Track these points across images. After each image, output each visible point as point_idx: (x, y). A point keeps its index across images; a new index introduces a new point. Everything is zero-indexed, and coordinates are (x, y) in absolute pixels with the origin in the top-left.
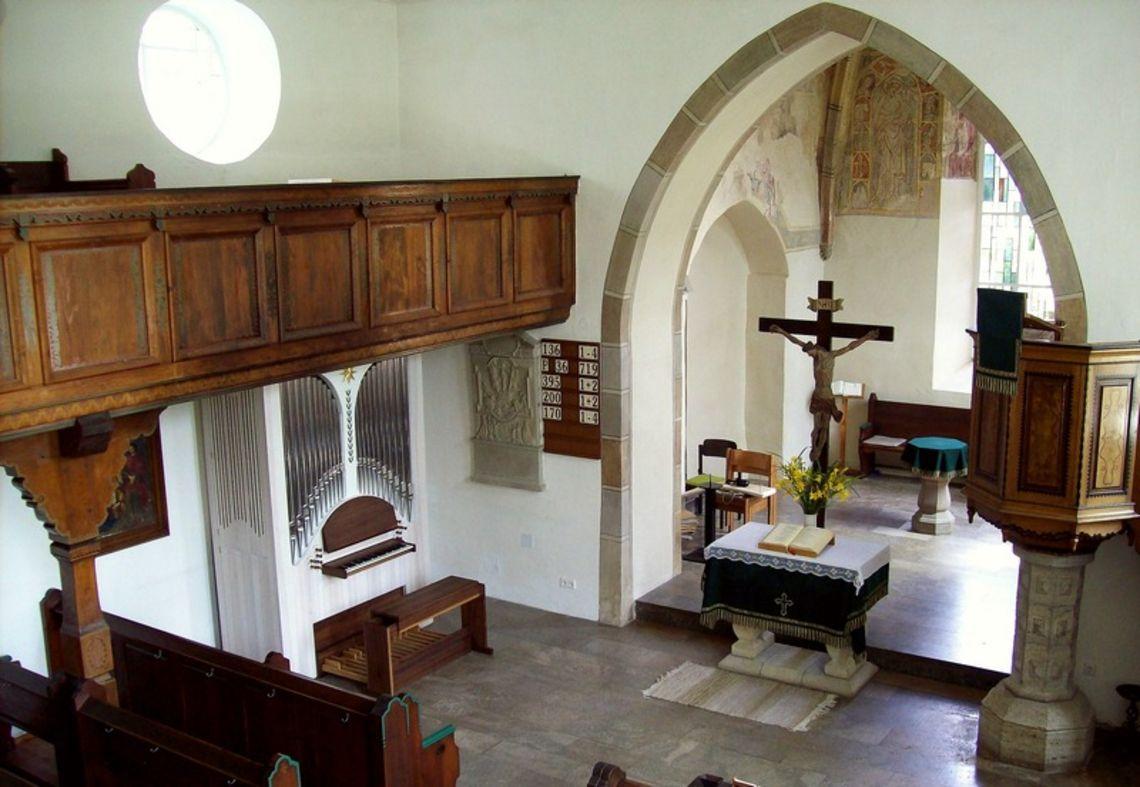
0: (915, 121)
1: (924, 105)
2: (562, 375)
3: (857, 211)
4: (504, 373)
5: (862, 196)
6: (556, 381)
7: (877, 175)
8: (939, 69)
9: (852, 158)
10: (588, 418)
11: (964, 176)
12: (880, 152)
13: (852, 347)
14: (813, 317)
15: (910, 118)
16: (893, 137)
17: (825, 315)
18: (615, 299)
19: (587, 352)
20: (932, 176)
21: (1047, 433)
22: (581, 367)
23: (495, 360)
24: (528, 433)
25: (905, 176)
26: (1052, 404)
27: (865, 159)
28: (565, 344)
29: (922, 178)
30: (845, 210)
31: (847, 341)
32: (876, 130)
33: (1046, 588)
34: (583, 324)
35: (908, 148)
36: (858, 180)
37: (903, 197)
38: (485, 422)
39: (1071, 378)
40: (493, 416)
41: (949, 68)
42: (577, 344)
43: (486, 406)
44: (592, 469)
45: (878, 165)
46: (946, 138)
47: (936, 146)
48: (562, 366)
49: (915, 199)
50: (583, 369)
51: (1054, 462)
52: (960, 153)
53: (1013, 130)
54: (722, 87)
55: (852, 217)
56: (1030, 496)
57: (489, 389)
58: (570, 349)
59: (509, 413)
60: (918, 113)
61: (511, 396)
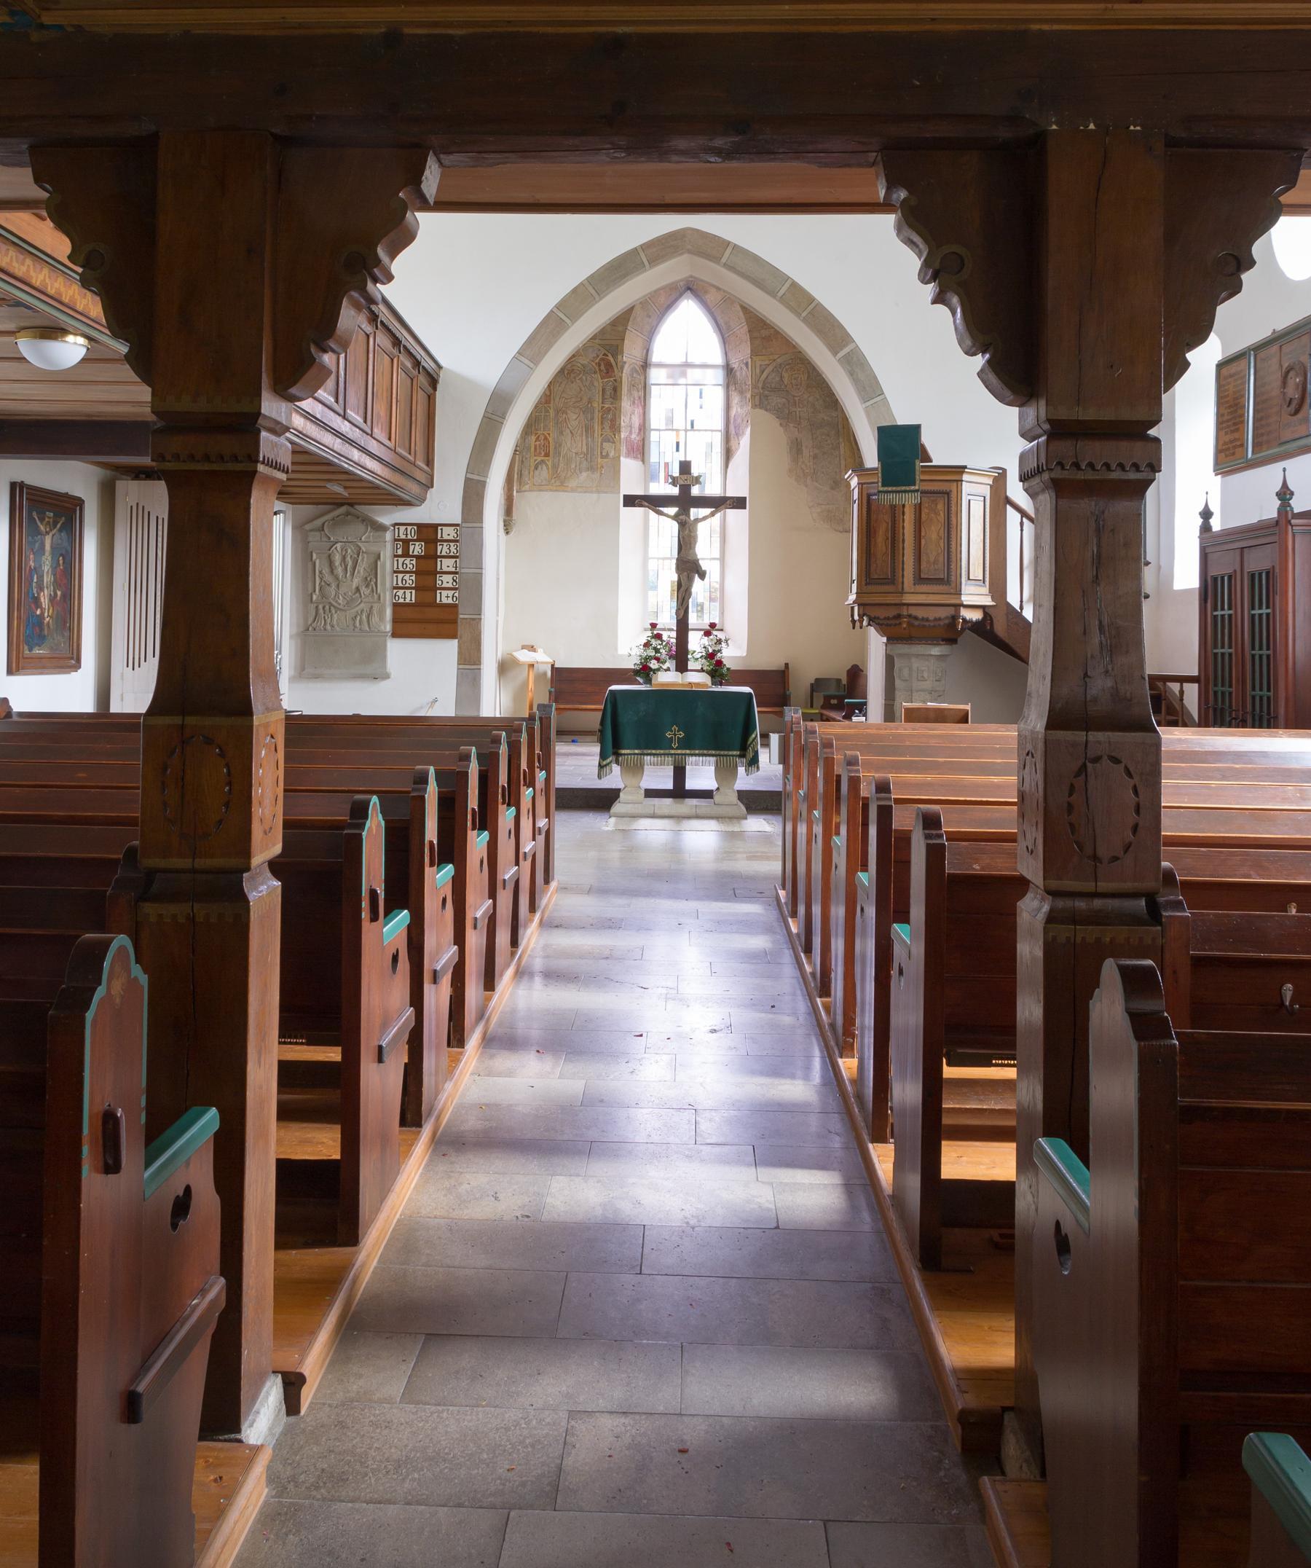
0: (595, 405)
1: (603, 390)
2: (417, 557)
3: (540, 488)
4: (348, 558)
5: (544, 473)
6: (410, 564)
7: (558, 453)
8: (787, 285)
9: (534, 438)
10: (445, 597)
11: (635, 458)
12: (561, 433)
13: (713, 514)
14: (675, 491)
15: (590, 402)
16: (574, 419)
17: (685, 489)
18: (479, 481)
19: (448, 533)
20: (612, 454)
21: (934, 536)
22: (439, 548)
23: (338, 545)
24: (375, 619)
25: (586, 455)
26: (937, 514)
27: (546, 438)
28: (421, 527)
29: (602, 457)
30: (527, 487)
31: (707, 511)
32: (557, 412)
33: (925, 675)
34: (441, 505)
35: (588, 429)
36: (539, 459)
37: (584, 474)
38: (321, 611)
39: (948, 494)
40: (331, 604)
41: (794, 285)
42: (435, 527)
43: (323, 595)
44: (448, 649)
45: (558, 445)
46: (624, 421)
47: (615, 428)
48: (417, 549)
49: (596, 475)
50: (443, 549)
51: (941, 559)
52: (633, 436)
53: (848, 335)
54: (593, 292)
55: (535, 494)
56: (924, 588)
57: (328, 578)
58: (428, 533)
59: (352, 600)
60: (598, 398)
61: (356, 581)
